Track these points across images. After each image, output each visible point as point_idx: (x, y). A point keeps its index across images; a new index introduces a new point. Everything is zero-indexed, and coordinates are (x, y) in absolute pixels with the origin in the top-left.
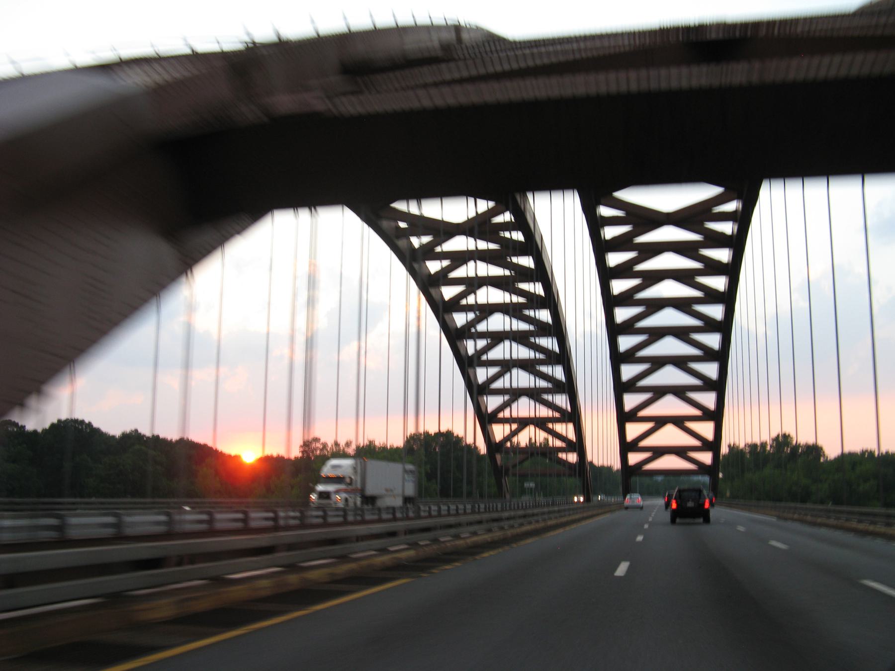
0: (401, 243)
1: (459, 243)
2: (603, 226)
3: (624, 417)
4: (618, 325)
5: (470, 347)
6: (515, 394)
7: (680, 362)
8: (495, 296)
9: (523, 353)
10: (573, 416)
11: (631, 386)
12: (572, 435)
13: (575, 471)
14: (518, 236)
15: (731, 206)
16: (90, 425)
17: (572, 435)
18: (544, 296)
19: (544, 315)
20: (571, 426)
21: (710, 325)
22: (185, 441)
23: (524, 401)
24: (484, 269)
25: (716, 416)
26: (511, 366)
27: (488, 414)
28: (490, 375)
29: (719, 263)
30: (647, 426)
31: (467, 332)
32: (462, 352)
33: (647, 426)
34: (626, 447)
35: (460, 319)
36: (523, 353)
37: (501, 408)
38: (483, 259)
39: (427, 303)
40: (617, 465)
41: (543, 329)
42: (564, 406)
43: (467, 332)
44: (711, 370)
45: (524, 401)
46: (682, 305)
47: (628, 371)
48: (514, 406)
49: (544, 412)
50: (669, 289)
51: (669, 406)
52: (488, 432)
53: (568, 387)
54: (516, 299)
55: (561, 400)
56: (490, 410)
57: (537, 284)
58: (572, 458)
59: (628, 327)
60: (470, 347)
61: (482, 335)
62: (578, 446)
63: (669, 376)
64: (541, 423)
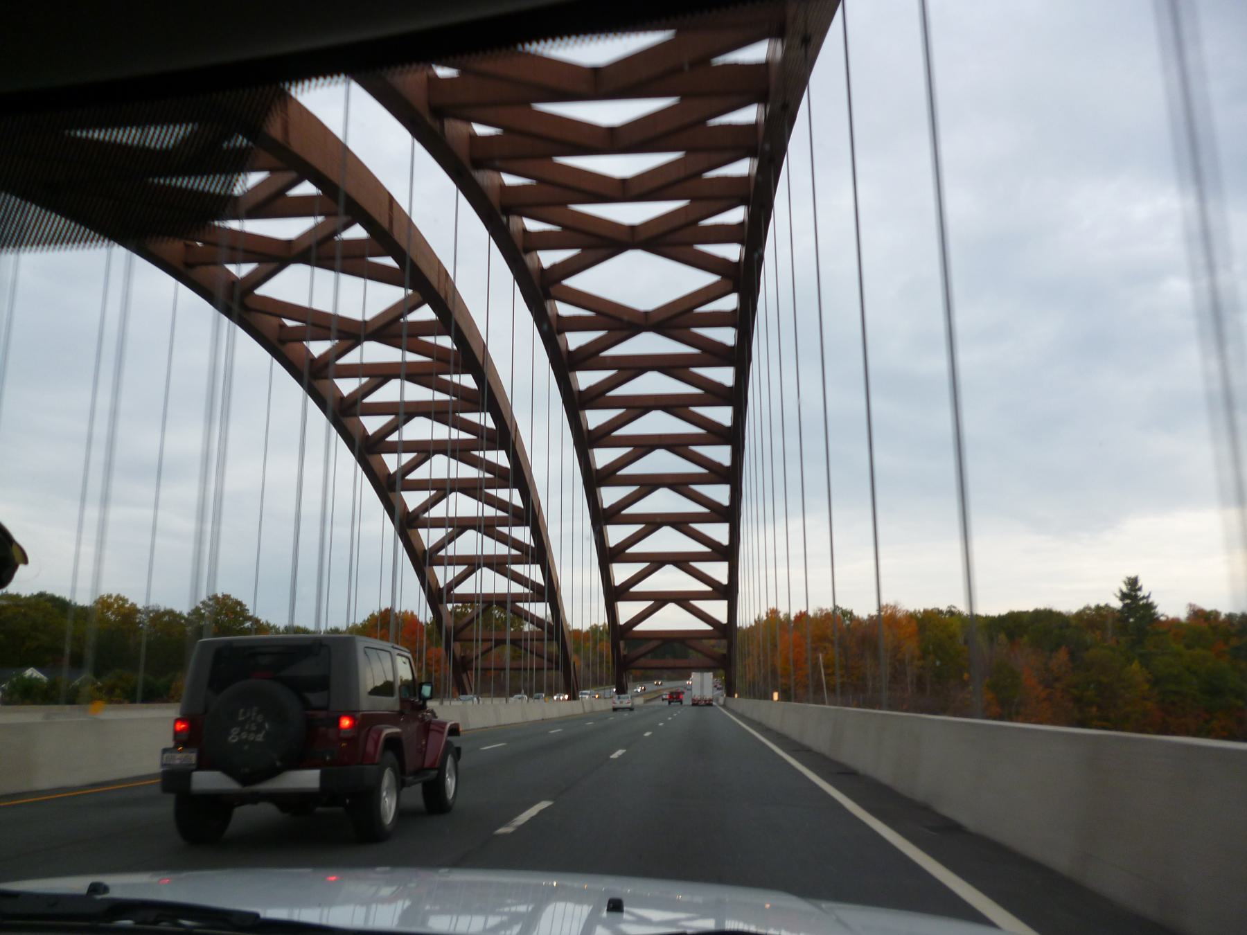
1: (374, 352)
2: (562, 331)
3: (608, 556)
4: (621, 626)
6: (460, 526)
7: (680, 523)
9: (492, 547)
10: (539, 553)
11: (609, 476)
12: (539, 579)
13: (557, 663)
15: (730, 302)
17: (539, 579)
18: (522, 506)
21: (716, 434)
22: (72, 606)
23: (470, 534)
24: (417, 393)
25: (728, 592)
26: (482, 564)
28: (396, 434)
29: (721, 346)
30: (643, 605)
33: (643, 605)
34: (614, 594)
36: (492, 547)
37: (442, 545)
38: (427, 415)
40: (602, 619)
42: (527, 542)
44: (720, 494)
45: (487, 573)
46: (676, 445)
47: (610, 496)
48: (458, 540)
50: (652, 383)
51: (663, 501)
53: (530, 515)
54: (490, 511)
55: (522, 534)
57: (533, 566)
58: (540, 610)
59: (603, 437)
63: (663, 501)
64: (498, 565)
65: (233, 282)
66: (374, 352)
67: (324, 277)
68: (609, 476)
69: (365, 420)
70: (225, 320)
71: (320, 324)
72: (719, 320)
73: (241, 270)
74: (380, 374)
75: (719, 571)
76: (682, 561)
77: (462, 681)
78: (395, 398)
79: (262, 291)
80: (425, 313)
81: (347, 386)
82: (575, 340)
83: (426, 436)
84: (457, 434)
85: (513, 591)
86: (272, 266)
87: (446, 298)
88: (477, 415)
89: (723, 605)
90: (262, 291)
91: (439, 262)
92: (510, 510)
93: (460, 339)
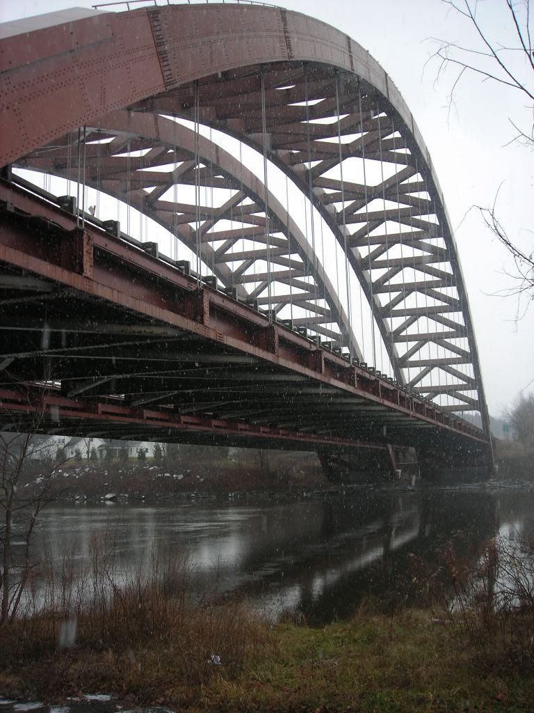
0: (296, 168)
5: (364, 251)
8: (392, 228)
9: (421, 277)
12: (467, 348)
14: (424, 195)
16: (112, 221)
17: (467, 348)
19: (446, 267)
20: (455, 289)
23: (423, 319)
27: (373, 283)
31: (370, 263)
32: (357, 257)
35: (376, 275)
36: (421, 277)
39: (323, 220)
41: (438, 255)
43: (370, 263)
49: (432, 302)
52: (343, 248)
56: (374, 280)
60: (364, 251)
61: (374, 241)
62: (480, 405)
65: (148, 196)
66: (223, 225)
67: (190, 189)
68: (379, 287)
69: (229, 264)
70: (144, 216)
71: (192, 212)
72: (416, 187)
73: (149, 190)
74: (233, 237)
75: (462, 343)
76: (438, 339)
77: (313, 99)
78: (240, 250)
79: (161, 199)
80: (248, 201)
81: (216, 245)
82: (339, 207)
83: (228, 228)
84: (297, 291)
85: (293, 293)
86: (164, 187)
87: (257, 192)
88: (303, 278)
89: (471, 366)
90: (161, 199)
91: (251, 173)
92: (342, 187)
93: (270, 213)
